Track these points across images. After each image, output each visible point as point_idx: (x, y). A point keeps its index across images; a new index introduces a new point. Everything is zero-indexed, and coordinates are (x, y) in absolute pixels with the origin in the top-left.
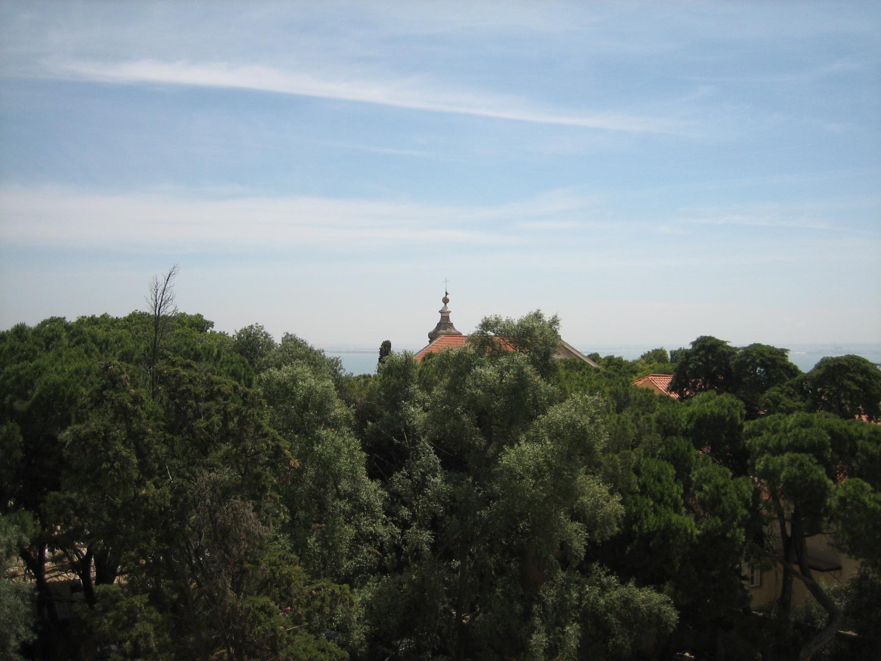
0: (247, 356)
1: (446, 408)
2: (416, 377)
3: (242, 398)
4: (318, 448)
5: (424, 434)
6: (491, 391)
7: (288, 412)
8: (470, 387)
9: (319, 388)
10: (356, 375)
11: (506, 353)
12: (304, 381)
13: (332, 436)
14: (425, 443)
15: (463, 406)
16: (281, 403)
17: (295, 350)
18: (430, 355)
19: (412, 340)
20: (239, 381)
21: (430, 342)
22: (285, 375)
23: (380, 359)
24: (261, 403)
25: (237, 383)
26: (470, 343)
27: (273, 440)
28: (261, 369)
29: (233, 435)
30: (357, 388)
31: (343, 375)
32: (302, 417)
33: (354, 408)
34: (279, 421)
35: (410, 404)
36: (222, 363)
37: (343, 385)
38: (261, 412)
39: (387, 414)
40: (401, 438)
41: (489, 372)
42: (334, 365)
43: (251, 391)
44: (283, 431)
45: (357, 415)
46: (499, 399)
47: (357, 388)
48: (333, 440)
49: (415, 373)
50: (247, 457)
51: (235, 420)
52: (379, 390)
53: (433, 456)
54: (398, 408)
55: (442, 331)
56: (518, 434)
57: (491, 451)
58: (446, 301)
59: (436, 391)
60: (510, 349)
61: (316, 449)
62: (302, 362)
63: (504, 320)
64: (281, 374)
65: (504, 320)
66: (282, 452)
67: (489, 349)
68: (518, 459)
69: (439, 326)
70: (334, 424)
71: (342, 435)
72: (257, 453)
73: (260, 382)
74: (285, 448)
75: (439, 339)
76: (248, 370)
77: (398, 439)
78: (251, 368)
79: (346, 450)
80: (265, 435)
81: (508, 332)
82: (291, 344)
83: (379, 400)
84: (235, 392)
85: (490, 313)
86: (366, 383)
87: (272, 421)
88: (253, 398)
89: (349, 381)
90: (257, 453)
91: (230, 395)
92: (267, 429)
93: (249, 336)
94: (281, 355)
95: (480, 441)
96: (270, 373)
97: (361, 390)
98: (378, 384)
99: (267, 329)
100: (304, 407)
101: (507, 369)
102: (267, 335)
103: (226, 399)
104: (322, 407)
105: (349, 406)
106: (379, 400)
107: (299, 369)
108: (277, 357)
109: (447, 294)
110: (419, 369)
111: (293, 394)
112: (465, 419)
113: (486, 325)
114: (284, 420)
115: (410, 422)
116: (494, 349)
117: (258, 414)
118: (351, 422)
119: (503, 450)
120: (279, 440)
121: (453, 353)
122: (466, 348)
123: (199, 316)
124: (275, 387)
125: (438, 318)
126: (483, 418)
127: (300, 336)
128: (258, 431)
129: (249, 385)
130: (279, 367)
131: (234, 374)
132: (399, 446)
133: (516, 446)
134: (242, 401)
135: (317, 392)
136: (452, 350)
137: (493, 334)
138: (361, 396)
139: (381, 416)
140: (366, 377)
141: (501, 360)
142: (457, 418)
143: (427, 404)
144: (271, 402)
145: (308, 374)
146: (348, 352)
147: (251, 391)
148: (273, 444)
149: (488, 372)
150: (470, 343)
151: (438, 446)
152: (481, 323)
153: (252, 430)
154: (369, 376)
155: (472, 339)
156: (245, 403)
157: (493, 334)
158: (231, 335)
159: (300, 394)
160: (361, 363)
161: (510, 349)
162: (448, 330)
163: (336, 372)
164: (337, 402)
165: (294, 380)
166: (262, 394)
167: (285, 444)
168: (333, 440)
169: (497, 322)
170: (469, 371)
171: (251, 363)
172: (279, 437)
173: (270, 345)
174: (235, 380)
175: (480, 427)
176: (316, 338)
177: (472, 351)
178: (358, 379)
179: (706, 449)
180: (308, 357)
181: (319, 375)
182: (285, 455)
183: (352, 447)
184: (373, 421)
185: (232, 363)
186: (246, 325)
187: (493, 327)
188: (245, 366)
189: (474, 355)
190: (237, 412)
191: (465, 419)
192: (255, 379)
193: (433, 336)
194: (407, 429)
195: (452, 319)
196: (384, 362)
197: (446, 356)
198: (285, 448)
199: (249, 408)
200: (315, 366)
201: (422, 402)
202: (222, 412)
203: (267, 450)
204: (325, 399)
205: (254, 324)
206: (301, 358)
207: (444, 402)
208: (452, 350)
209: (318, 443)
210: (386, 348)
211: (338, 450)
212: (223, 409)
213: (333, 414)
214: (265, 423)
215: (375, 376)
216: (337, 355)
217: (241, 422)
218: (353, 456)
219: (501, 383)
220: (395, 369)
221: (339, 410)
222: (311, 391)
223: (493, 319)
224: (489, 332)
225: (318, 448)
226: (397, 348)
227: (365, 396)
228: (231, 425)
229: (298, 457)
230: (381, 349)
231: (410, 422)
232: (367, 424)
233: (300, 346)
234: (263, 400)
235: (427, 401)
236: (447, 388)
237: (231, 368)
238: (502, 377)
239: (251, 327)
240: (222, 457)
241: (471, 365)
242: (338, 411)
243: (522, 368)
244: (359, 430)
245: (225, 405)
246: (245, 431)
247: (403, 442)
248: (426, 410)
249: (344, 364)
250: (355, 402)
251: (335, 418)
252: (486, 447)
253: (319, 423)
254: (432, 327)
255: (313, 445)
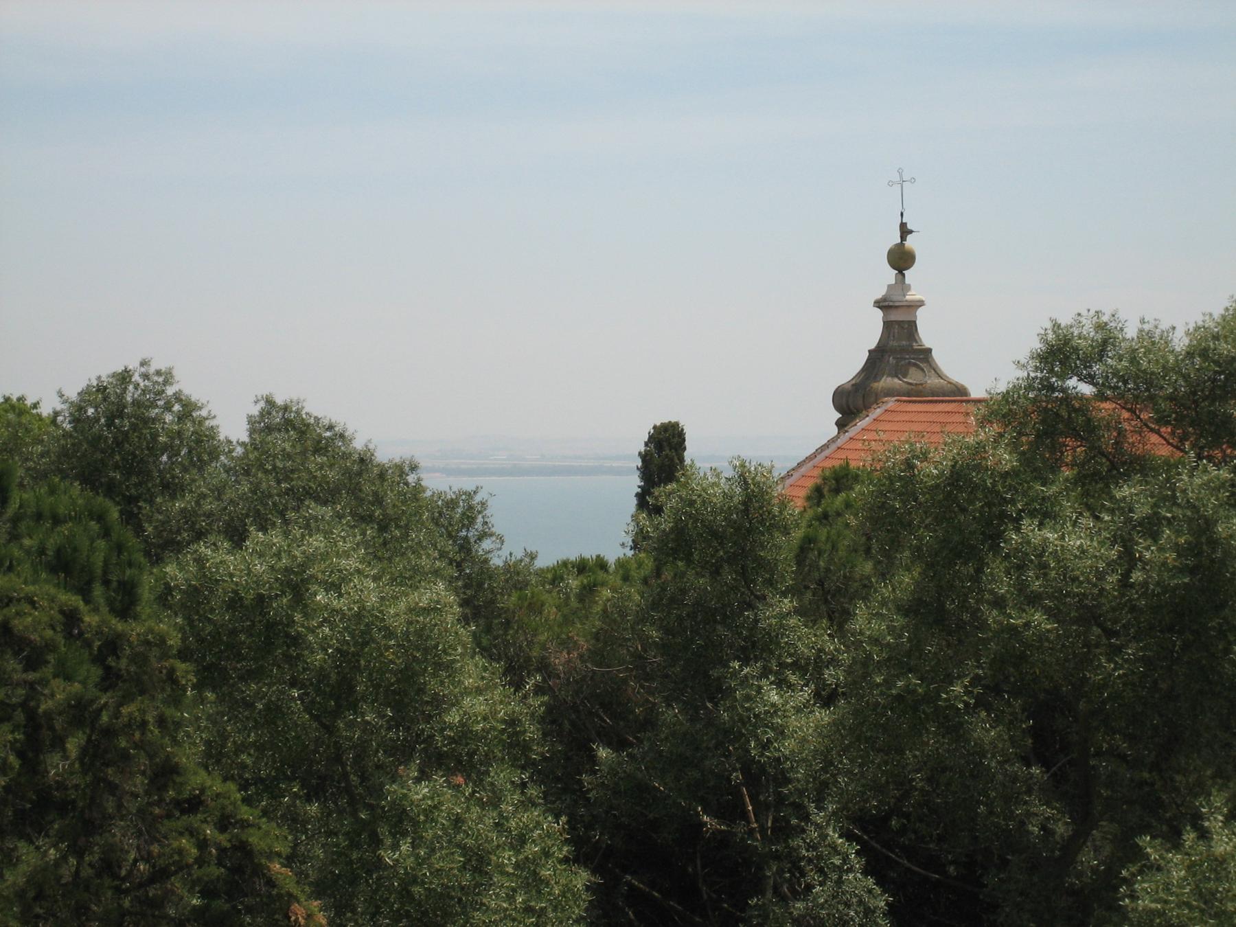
0: (111, 490)
1: (909, 690)
2: (788, 571)
3: (99, 659)
4: (398, 855)
5: (821, 793)
6: (1085, 614)
7: (274, 712)
8: (999, 603)
9: (396, 614)
10: (546, 560)
11: (1140, 466)
12: (334, 587)
13: (451, 804)
14: (826, 832)
15: (976, 680)
16: (253, 675)
17: (302, 464)
18: (840, 479)
19: (768, 417)
20: (85, 592)
21: (841, 425)
22: (259, 568)
23: (642, 498)
24: (171, 678)
25: (75, 601)
26: (996, 428)
27: (224, 824)
28: (166, 546)
29: (64, 807)
30: (551, 612)
31: (497, 561)
32: (330, 729)
33: (539, 690)
34: (239, 749)
35: (765, 673)
36: (16, 520)
37: (496, 603)
38: (170, 712)
39: (672, 714)
40: (731, 811)
41: (1073, 540)
42: (458, 521)
43: (134, 630)
44: (262, 788)
45: (551, 719)
46: (1118, 650)
47: (551, 612)
48: (458, 822)
49: (782, 550)
50: (118, 890)
51: (73, 745)
52: (642, 619)
53: (858, 882)
54: (717, 691)
55: (887, 382)
56: (1200, 789)
57: (1088, 859)
58: (901, 259)
59: (862, 620)
60: (1158, 446)
61: (388, 857)
62: (326, 512)
63: (1131, 332)
64: (242, 565)
65: (1131, 332)
66: (259, 871)
67: (1074, 450)
68: (1198, 892)
69: (877, 360)
70: (457, 758)
71: (495, 802)
72: (160, 875)
73: (164, 596)
74: (271, 855)
75: (877, 412)
76: (120, 548)
77: (718, 815)
78: (132, 541)
79: (508, 858)
80: (193, 804)
81: (1149, 380)
82: (282, 442)
83: (639, 657)
84: (69, 636)
85: (1072, 305)
86: (588, 591)
87: (214, 756)
88: (140, 660)
89: (521, 586)
90: (160, 875)
91: (50, 647)
92: (199, 779)
93: (116, 411)
94: (245, 488)
95: (1044, 817)
96: (200, 561)
97: (567, 621)
98: (635, 596)
99: (188, 384)
100: (336, 692)
101: (1151, 527)
102: (188, 408)
103: (33, 662)
104: (408, 689)
105: (518, 686)
106: (639, 657)
107: (317, 542)
108: (229, 494)
109: (905, 231)
110: (797, 534)
111: (296, 640)
112: (985, 731)
113: (1060, 354)
114: (260, 748)
115: (765, 746)
116: (1096, 451)
117: (161, 721)
118: (526, 748)
119: (1137, 854)
120: (244, 825)
121: (929, 470)
122: (980, 448)
123: (677, 424)
124: (222, 616)
125: (869, 330)
126: (1055, 726)
127: (321, 406)
128: (163, 788)
129: (125, 605)
130: (237, 537)
131: (63, 565)
132: (723, 841)
133: (1189, 837)
134: (96, 672)
135: (389, 633)
136: (924, 457)
137: (1086, 389)
138: (566, 644)
139: (649, 722)
140: (589, 569)
141: (1125, 491)
142: (952, 726)
143: (829, 675)
144: (210, 676)
145: (351, 563)
146: (516, 471)
147: (134, 630)
148: (223, 839)
149: (1074, 542)
150: (996, 428)
151: (876, 837)
152: (1037, 345)
153: (139, 783)
154: (601, 564)
155: (1003, 410)
156: (110, 679)
157: (1086, 389)
158: (45, 410)
159: (321, 644)
160: (563, 507)
161: (1158, 446)
162: (914, 377)
163: (465, 547)
164: (473, 671)
165: (295, 585)
166: (174, 641)
167: (268, 837)
168: (458, 822)
169: (1106, 340)
170: (994, 538)
171: (131, 518)
172: (246, 813)
173: (203, 444)
174: (67, 587)
175: (1046, 764)
176: (380, 420)
177: (1006, 459)
178: (555, 576)
179: (23, 847)
180: (355, 491)
181: (400, 565)
182: (271, 883)
183: (533, 849)
184: (618, 744)
185: (57, 520)
186: (102, 368)
187: (1087, 362)
188: (106, 533)
189: (1014, 473)
190: (80, 713)
191: (985, 731)
192: (147, 585)
193: (851, 403)
194: (755, 775)
195: (929, 332)
196: (658, 510)
197: (903, 480)
198: (271, 855)
199: (126, 698)
200: (383, 528)
201: (812, 667)
202: (20, 716)
203: (200, 862)
204: (423, 650)
205: (133, 364)
206: (326, 495)
207: (899, 661)
208: (924, 457)
209: (398, 832)
210: (665, 450)
211: (478, 861)
212: (24, 705)
213: (453, 717)
214: (188, 755)
215: (622, 564)
216: (467, 484)
217: (94, 755)
218: (534, 883)
219: (1124, 583)
220: (705, 538)
221: (478, 698)
222: (364, 627)
223: (1088, 329)
224: (1072, 382)
225: (398, 855)
226: (709, 454)
227: (584, 644)
228: (56, 766)
229: (319, 890)
230: (645, 457)
231: (765, 746)
232: (592, 758)
233: (320, 447)
234: (181, 667)
235: (834, 662)
236: (905, 610)
237: (52, 543)
238: (1129, 559)
239: (124, 377)
240: (21, 894)
241: (1003, 516)
242: (477, 705)
243: (1210, 524)
244: (560, 781)
245: (31, 685)
246: (113, 788)
247: (740, 828)
248: (826, 698)
249: (499, 517)
250: (544, 667)
251: (464, 734)
252: (1071, 847)
253: (403, 752)
254: (849, 367)
255: (376, 842)
